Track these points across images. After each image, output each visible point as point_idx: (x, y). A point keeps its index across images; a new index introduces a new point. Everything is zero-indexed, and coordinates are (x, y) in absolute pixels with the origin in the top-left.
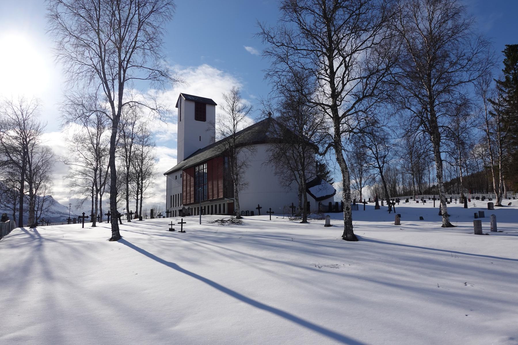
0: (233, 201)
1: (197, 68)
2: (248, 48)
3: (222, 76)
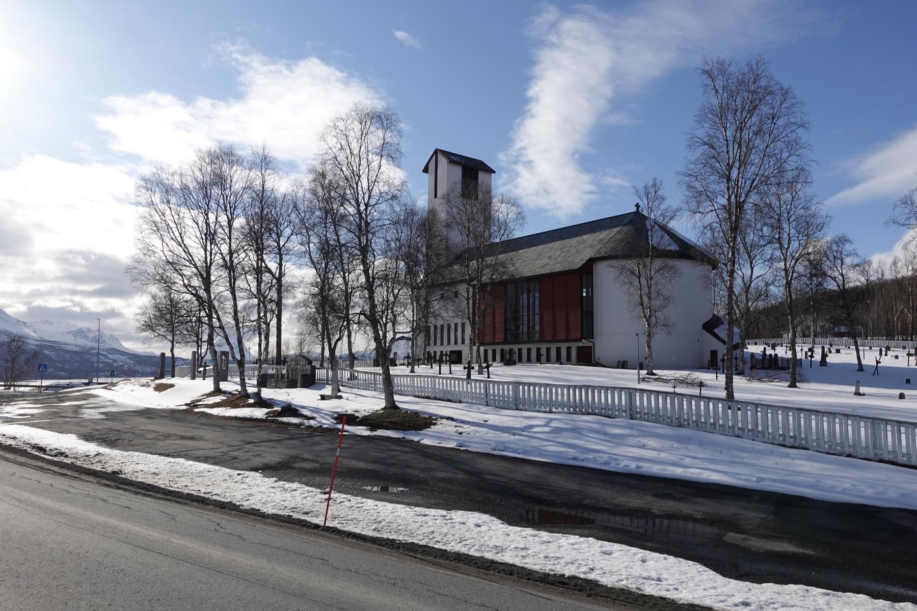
1: (297, 65)
2: (400, 35)
3: (346, 83)
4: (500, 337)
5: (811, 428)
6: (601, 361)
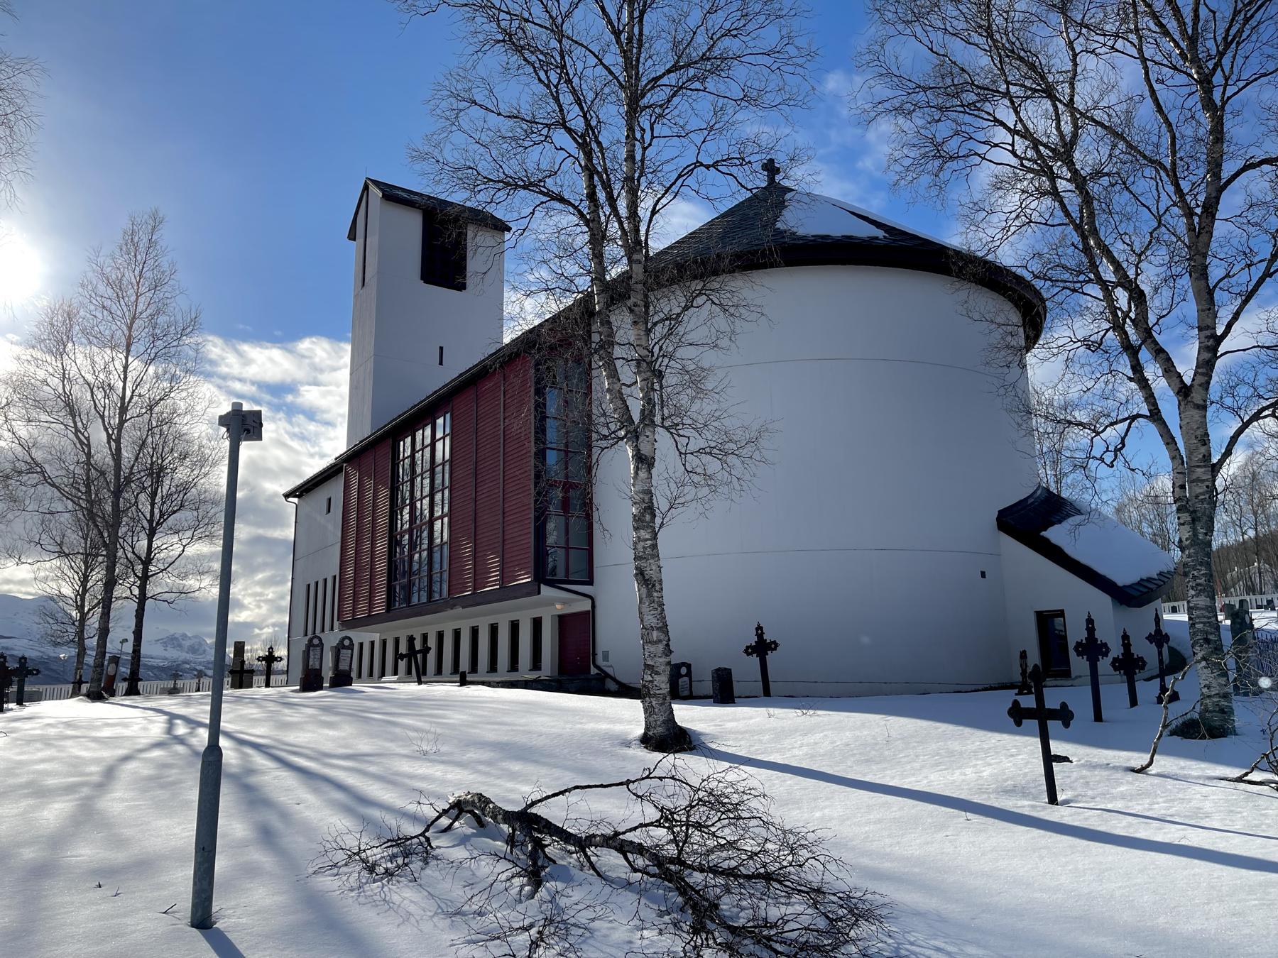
0: (585, 606)
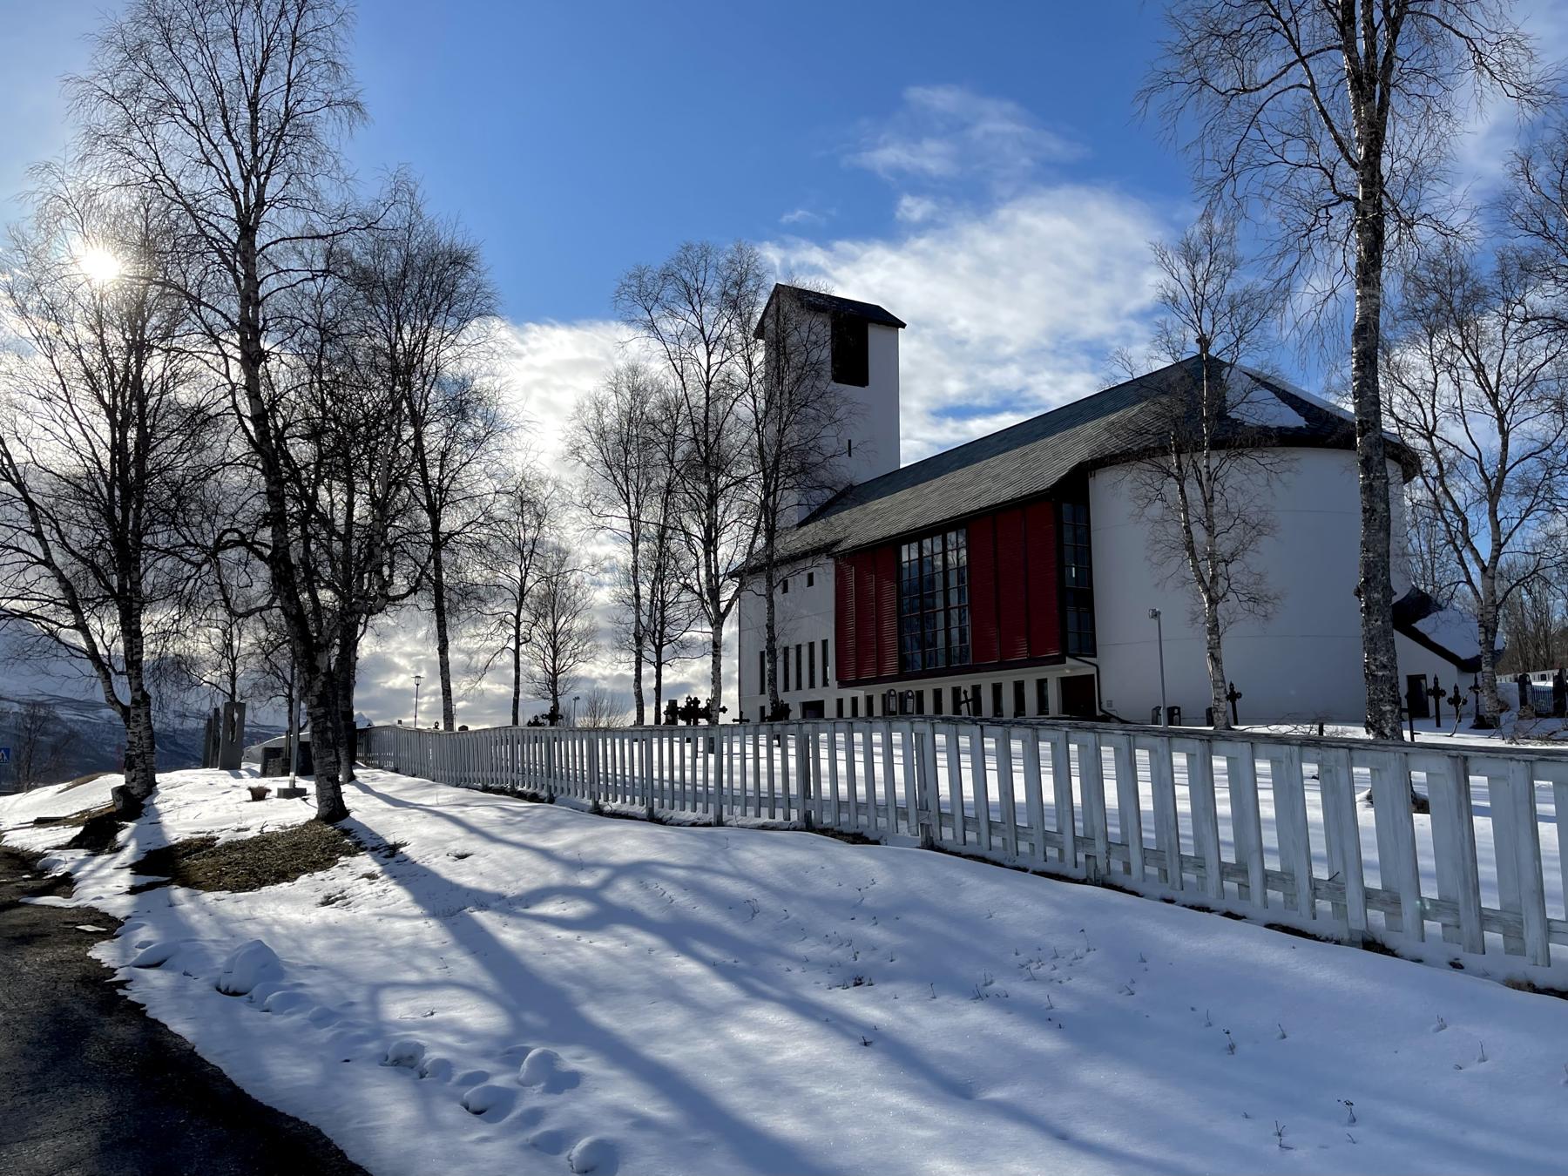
4: (891, 666)
5: (1277, 789)
6: (1118, 709)
